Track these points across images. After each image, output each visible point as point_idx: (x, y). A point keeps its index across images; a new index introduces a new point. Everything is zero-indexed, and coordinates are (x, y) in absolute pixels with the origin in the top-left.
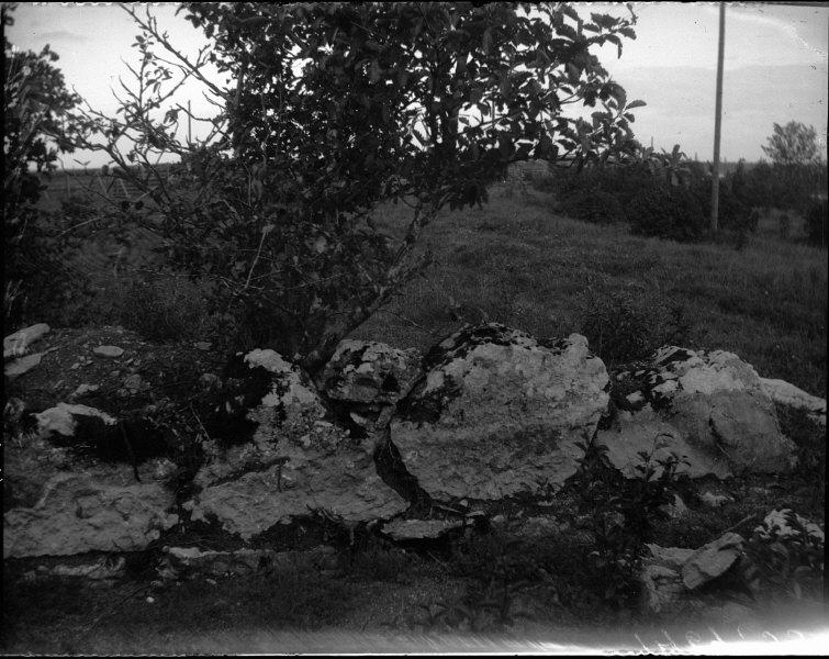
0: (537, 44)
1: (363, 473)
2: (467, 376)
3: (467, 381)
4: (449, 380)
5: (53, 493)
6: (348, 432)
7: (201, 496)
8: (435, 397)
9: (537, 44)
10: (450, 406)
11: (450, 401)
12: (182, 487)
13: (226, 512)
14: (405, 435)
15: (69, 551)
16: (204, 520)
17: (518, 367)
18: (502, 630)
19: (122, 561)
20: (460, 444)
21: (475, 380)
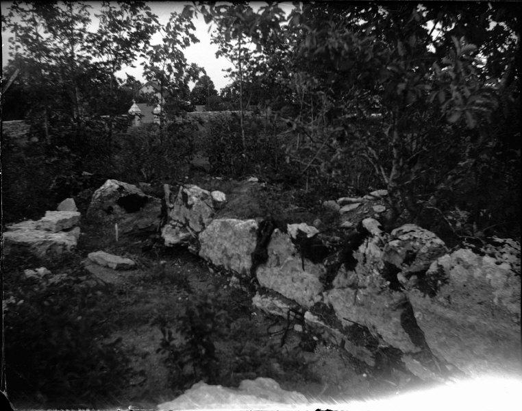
0: (453, 25)
1: (393, 314)
2: (453, 271)
3: (453, 274)
4: (441, 267)
5: (286, 264)
6: (389, 283)
7: (331, 291)
8: (432, 278)
9: (453, 25)
10: (442, 288)
11: (442, 285)
12: (327, 282)
13: (337, 307)
14: (418, 299)
15: (287, 296)
16: (327, 305)
17: (489, 276)
18: (388, 374)
19: (519, 97)
20: (448, 320)
21: (457, 275)
